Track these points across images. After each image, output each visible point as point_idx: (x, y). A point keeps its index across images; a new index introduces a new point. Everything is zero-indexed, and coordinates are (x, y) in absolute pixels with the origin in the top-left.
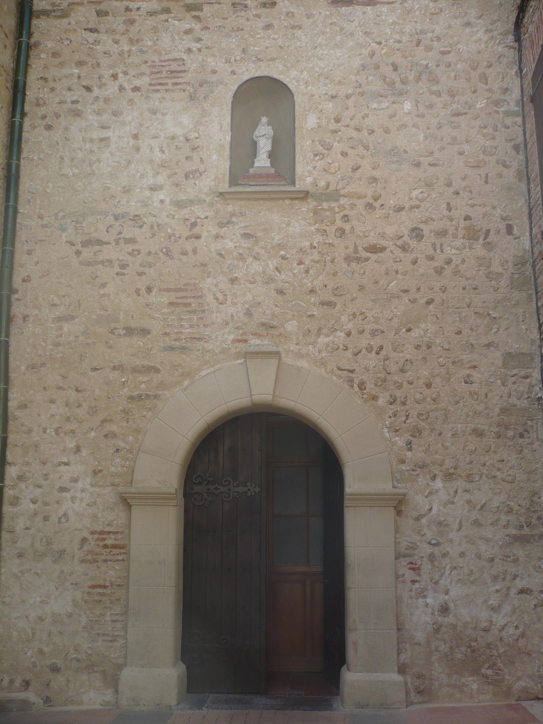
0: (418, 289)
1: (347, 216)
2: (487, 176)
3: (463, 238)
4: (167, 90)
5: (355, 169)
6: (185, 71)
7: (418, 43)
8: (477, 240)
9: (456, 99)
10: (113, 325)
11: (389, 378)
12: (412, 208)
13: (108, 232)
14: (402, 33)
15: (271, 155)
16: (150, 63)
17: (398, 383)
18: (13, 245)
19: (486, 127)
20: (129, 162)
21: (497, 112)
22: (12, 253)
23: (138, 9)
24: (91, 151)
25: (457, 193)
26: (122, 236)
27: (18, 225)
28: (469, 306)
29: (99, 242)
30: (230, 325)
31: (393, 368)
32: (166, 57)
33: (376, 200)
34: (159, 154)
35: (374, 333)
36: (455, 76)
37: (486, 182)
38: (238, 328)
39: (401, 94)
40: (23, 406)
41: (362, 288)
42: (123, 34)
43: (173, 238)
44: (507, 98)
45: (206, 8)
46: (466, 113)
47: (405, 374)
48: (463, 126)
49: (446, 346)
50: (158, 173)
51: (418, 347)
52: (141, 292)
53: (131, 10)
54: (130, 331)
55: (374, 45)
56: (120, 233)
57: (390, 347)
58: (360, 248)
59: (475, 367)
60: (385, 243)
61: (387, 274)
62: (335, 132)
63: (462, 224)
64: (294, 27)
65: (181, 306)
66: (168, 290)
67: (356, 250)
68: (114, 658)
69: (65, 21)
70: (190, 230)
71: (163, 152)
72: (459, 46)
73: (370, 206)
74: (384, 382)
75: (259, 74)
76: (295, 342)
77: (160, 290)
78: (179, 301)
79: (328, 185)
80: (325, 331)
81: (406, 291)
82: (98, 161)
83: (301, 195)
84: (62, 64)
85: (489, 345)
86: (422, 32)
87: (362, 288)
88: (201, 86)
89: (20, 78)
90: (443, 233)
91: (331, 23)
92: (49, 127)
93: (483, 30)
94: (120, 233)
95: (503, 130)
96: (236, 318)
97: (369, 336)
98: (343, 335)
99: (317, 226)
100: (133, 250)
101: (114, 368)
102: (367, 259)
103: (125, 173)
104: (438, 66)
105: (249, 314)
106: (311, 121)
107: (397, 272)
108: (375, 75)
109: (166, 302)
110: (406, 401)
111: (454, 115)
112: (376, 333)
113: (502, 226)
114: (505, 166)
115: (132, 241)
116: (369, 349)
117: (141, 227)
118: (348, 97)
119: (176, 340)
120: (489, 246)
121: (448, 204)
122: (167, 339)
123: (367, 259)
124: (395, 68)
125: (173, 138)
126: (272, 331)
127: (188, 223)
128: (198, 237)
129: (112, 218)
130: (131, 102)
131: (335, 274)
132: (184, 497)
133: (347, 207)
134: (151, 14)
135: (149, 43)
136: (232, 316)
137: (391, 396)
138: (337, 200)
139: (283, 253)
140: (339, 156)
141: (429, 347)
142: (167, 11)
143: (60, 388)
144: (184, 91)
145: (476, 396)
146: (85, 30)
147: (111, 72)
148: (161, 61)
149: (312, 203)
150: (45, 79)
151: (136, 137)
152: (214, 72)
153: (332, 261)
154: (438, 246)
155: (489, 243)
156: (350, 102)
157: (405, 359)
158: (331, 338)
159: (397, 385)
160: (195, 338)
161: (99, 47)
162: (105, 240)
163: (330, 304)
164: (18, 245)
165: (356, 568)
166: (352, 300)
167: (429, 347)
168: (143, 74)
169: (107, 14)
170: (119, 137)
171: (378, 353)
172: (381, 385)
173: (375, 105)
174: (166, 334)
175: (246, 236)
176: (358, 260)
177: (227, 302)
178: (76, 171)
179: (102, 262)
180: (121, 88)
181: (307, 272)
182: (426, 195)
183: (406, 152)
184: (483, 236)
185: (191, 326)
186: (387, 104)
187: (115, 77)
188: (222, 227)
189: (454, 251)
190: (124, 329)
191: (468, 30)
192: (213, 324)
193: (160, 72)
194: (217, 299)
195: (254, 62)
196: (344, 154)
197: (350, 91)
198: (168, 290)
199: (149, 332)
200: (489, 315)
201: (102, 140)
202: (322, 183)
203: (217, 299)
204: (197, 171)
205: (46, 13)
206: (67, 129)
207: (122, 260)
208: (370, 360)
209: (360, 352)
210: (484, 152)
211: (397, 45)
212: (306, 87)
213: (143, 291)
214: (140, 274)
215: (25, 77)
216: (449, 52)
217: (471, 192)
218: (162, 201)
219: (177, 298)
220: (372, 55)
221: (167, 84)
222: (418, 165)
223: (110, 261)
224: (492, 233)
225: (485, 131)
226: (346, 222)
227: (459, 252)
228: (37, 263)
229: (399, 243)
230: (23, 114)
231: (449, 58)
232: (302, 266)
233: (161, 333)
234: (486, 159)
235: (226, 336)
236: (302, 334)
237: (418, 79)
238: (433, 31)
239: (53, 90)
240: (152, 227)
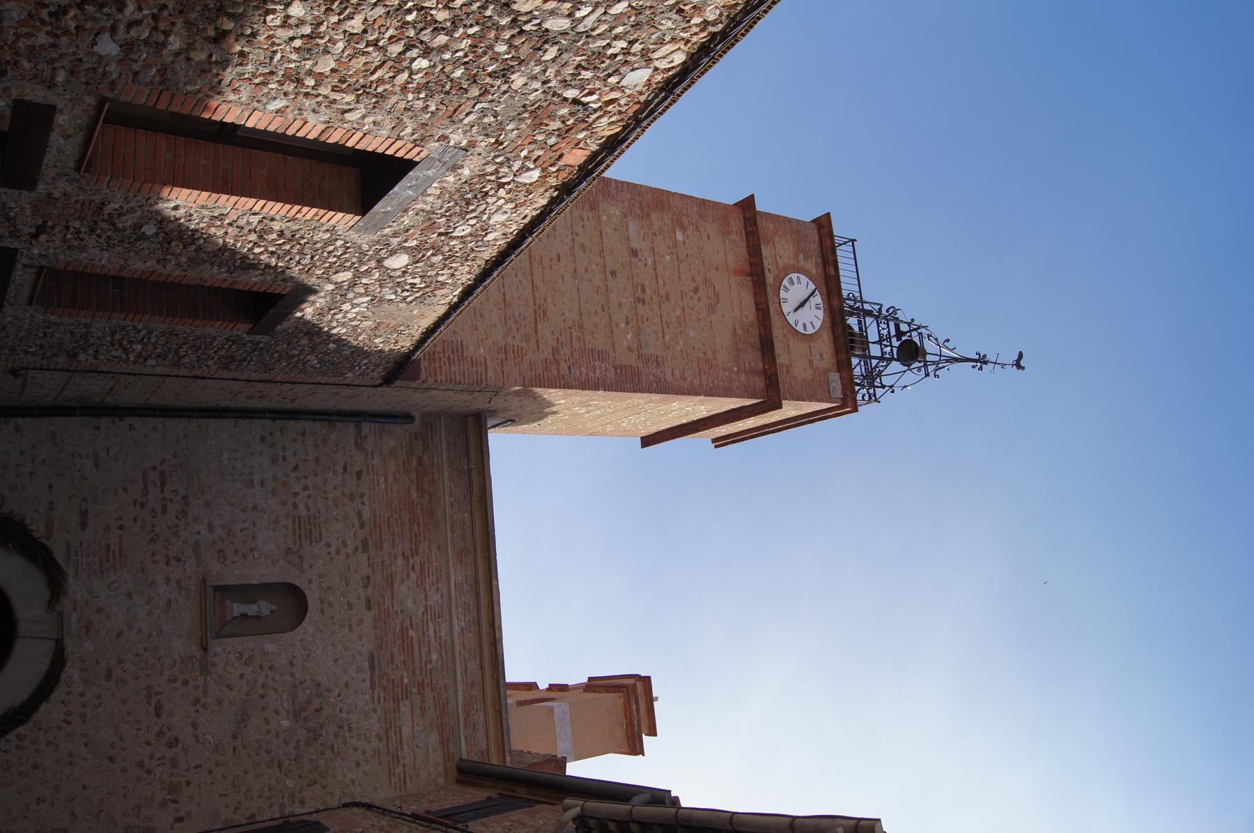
0: (124, 749)
1: (188, 683)
2: (226, 795)
3: (170, 782)
4: (295, 530)
5: (229, 687)
6: (311, 542)
7: (341, 727)
8: (169, 793)
9: (293, 762)
12: (196, 737)
13: (173, 491)
14: (349, 712)
15: (245, 615)
16: (317, 515)
18: (160, 416)
19: (269, 789)
20: (232, 505)
21: (283, 797)
22: (154, 416)
23: (363, 503)
24: (242, 474)
25: (210, 772)
26: (169, 503)
27: (178, 419)
28: (108, 793)
29: (163, 484)
32: (323, 528)
33: (202, 706)
34: (240, 528)
35: (83, 716)
36: (312, 760)
37: (221, 795)
39: (295, 717)
40: (17, 429)
41: (124, 702)
42: (342, 492)
43: (167, 543)
44: (296, 804)
45: (365, 556)
46: (281, 772)
48: (270, 771)
49: (71, 778)
50: (223, 528)
51: (70, 754)
53: (361, 498)
54: (84, 514)
55: (338, 691)
56: (171, 501)
58: (159, 697)
59: (52, 804)
60: (164, 716)
61: (136, 722)
62: (261, 667)
63: (183, 780)
64: (350, 626)
66: (121, 542)
67: (157, 694)
69: (353, 447)
70: (174, 557)
71: (242, 531)
72: (339, 760)
73: (197, 701)
75: (310, 601)
77: (120, 536)
78: (111, 552)
79: (215, 665)
81: (121, 739)
82: (234, 480)
83: (204, 645)
84: (316, 446)
85: (73, 814)
86: (350, 729)
87: (124, 702)
88: (299, 557)
89: (302, 416)
90: (174, 763)
91: (354, 655)
92: (263, 439)
93: (354, 777)
94: (171, 501)
95: (268, 804)
98: (81, 689)
99: (178, 660)
100: (156, 512)
101: (51, 503)
102: (149, 704)
103: (223, 502)
104: (321, 744)
105: (99, 610)
106: (270, 648)
107: (138, 729)
108: (311, 694)
111: (279, 762)
113: (182, 813)
114: (236, 810)
115: (165, 511)
116: (69, 713)
117: (177, 517)
118: (292, 675)
119: (76, 552)
120: (164, 804)
121: (200, 766)
123: (149, 704)
124: (318, 710)
125: (254, 538)
127: (180, 555)
128: (167, 564)
129: (184, 494)
130: (284, 503)
131: (136, 678)
133: (196, 683)
134: (359, 514)
135: (335, 513)
136: (97, 597)
137: (25, 736)
138: (201, 674)
139: (154, 634)
140: (241, 672)
141: (70, 763)
142: (362, 526)
143: (34, 460)
144: (294, 544)
145: (25, 808)
146: (346, 463)
147: (310, 485)
148: (319, 523)
149: (198, 654)
150: (303, 434)
151: (255, 508)
152: (311, 566)
153: (148, 676)
154: (162, 761)
155: (166, 804)
156: (287, 677)
161: (331, 473)
162: (165, 490)
163: (108, 677)
164: (161, 420)
166: (113, 695)
167: (70, 763)
168: (308, 510)
169: (359, 479)
170: (254, 495)
171: (64, 721)
173: (285, 697)
174: (81, 544)
175: (169, 603)
176: (149, 697)
178: (225, 463)
179: (146, 488)
180: (296, 494)
181: (137, 655)
182: (208, 746)
183: (245, 726)
184: (172, 797)
186: (286, 706)
187: (306, 488)
188: (177, 583)
189: (158, 775)
190: (87, 510)
191: (353, 765)
193: (310, 524)
194: (113, 583)
195: (320, 598)
196: (242, 676)
197: (297, 676)
198: (121, 542)
199: (83, 530)
200: (102, 811)
201: (252, 482)
202: (216, 660)
203: (113, 583)
204: (225, 559)
205: (359, 432)
206: (261, 453)
207: (147, 503)
209: (65, 705)
210: (247, 790)
211: (337, 710)
212: (299, 641)
213: (119, 523)
214: (135, 520)
215: (304, 419)
216: (334, 752)
217: (212, 783)
218: (199, 533)
220: (329, 691)
221: (300, 530)
222: (234, 737)
223: (147, 494)
224: (176, 805)
225: (266, 789)
226: (183, 683)
227: (158, 779)
228: (145, 435)
229: (165, 729)
230: (274, 419)
231: (328, 753)
232: (142, 650)
234: (242, 793)
237: (309, 730)
238: (351, 737)
239: (295, 440)
240: (176, 526)
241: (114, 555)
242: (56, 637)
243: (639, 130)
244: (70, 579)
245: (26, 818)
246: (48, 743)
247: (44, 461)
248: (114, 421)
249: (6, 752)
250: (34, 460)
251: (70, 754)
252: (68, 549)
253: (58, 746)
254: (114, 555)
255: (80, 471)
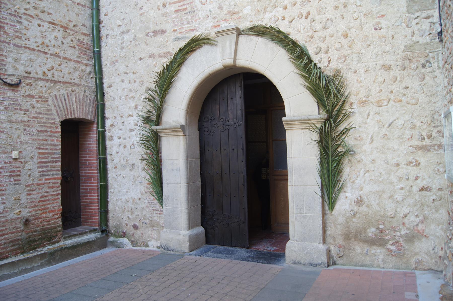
10: (147, 31)
11: (315, 35)
17: (322, 37)
30: (210, 17)
31: (318, 27)
38: (214, 18)
47: (327, 30)
52: (160, 7)
54: (155, 33)
57: (316, 12)
65: (181, 11)
68: (162, 223)
74: (312, 39)
76: (249, 20)
78: (181, 8)
80: (269, 9)
96: (213, 12)
97: (299, 7)
98: (281, 9)
101: (150, 57)
109: (174, 11)
110: (328, 50)
112: (305, 4)
119: (180, 33)
122: (175, 33)
126: (235, 16)
132: (198, 130)
136: (211, 11)
141: (345, 6)
143: (126, 73)
157: (326, 19)
158: (273, 13)
159: (321, 39)
160: (190, 30)
165: (293, 172)
167: (345, 6)
172: (309, 41)
174: (175, 31)
177: (208, 3)
185: (188, 23)
190: (153, 32)
192: (200, 18)
199: (165, 32)
208: (301, 24)
213: (161, 7)
219: (179, 6)
233: (172, 30)
235: (208, 25)
236: (254, 14)
241: (182, 6)
242: (235, 35)
243: (94, 7)
244: (197, 34)
245: (393, 37)
246: (325, 28)
247: (127, 66)
248: (103, 27)
249: (329, 61)
250: (126, 73)
251: (336, 8)
252: (178, 39)
253: (328, 19)
254: (182, 6)
255: (131, 42)
